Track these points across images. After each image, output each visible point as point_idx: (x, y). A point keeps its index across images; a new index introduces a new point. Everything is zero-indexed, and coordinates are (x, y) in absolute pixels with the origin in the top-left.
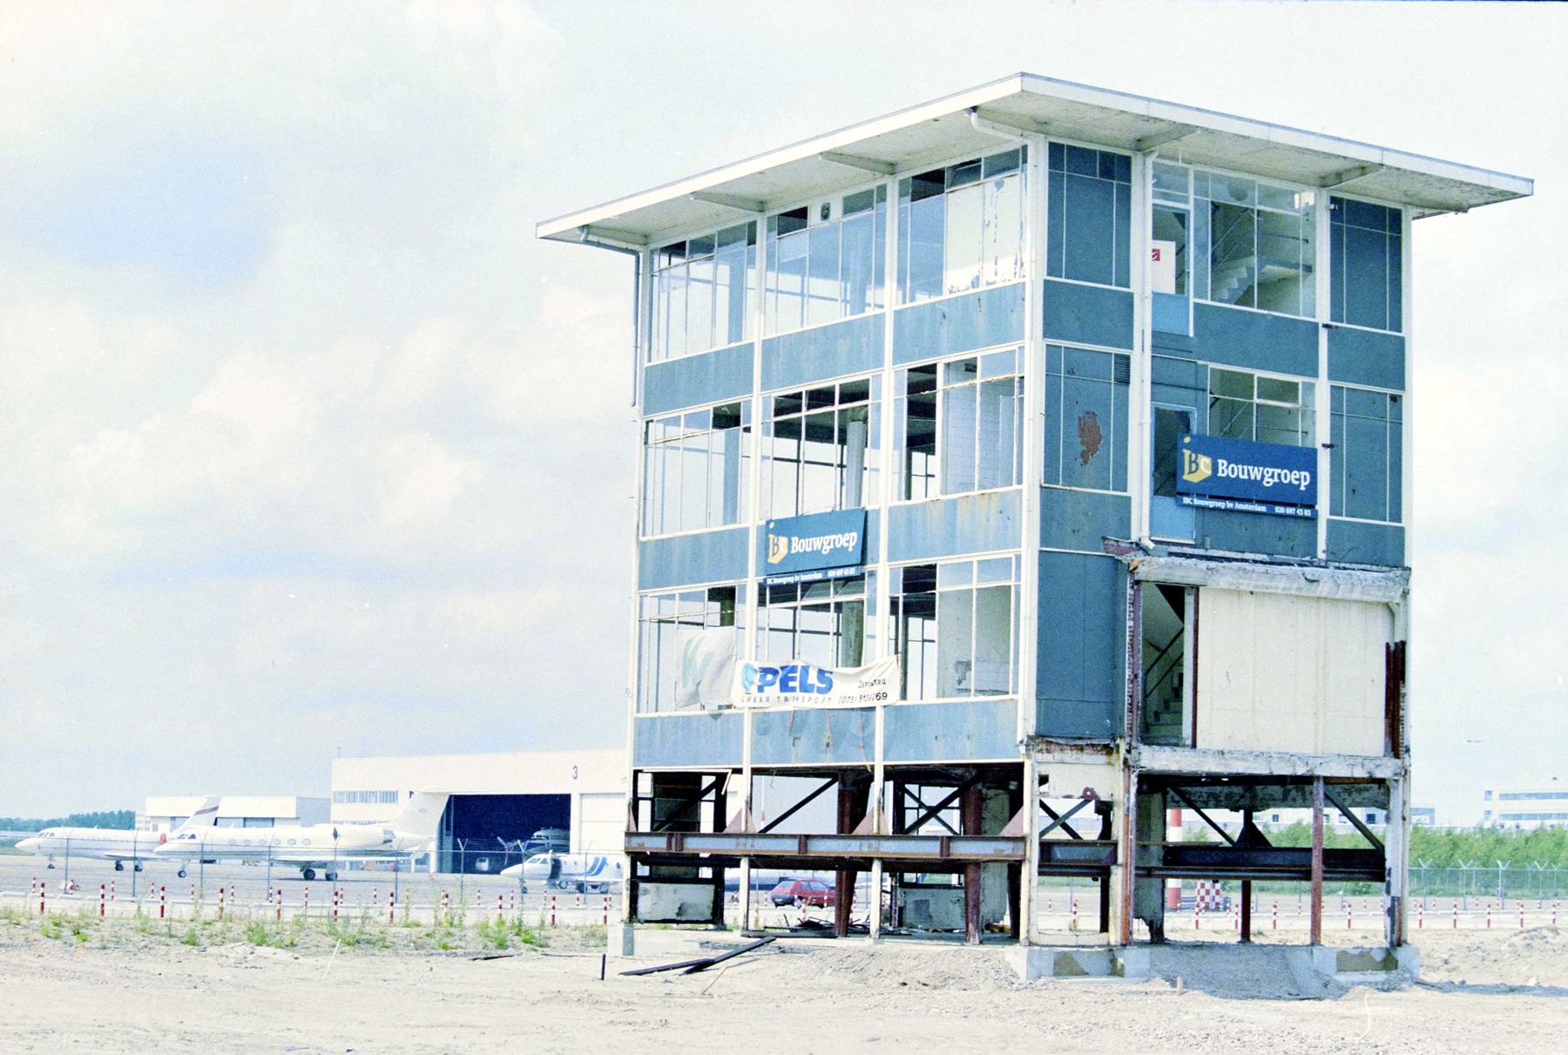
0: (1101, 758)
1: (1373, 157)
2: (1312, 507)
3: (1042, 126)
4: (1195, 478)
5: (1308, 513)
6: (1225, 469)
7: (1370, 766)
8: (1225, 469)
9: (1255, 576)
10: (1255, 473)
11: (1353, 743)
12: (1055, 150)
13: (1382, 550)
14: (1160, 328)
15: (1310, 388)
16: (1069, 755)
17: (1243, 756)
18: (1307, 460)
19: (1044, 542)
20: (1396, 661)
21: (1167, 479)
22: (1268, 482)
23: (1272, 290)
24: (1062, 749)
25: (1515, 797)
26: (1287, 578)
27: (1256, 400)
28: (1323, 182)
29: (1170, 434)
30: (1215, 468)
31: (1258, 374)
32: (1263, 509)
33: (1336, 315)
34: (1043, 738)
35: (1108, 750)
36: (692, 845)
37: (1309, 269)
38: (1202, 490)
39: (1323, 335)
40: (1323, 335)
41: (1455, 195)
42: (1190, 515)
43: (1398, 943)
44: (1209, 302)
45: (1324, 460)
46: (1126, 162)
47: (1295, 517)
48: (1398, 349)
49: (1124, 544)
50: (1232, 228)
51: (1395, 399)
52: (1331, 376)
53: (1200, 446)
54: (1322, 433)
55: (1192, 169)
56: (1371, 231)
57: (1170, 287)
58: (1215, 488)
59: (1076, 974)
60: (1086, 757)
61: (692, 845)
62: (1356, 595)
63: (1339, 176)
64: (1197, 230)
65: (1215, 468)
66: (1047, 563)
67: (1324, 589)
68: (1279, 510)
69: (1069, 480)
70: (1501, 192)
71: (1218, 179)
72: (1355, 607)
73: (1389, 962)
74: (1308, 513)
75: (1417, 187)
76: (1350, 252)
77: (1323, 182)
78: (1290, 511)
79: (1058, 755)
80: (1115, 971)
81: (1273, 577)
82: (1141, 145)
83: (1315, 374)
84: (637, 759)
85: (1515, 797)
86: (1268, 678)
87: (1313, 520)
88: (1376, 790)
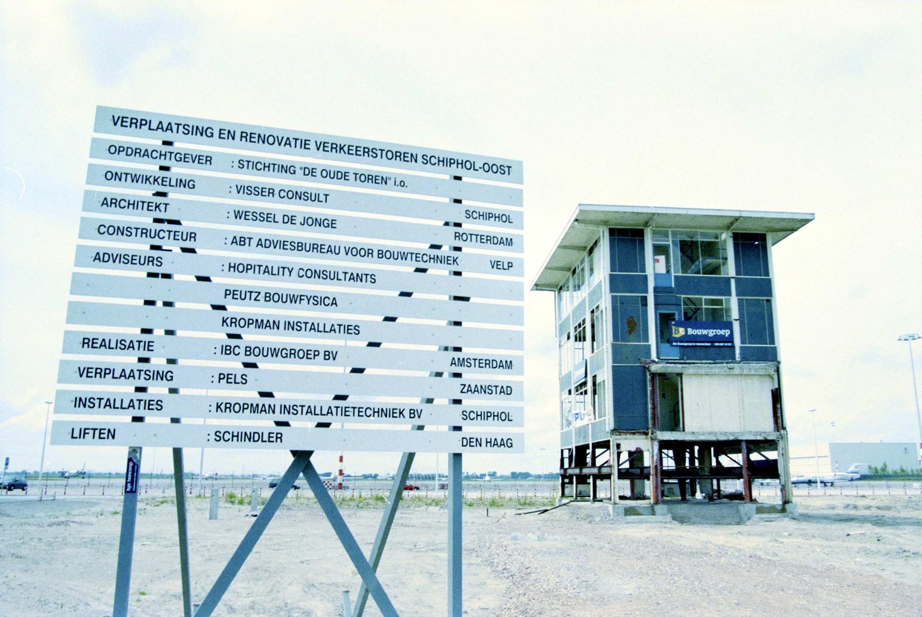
0: (644, 437)
1: (737, 214)
2: (732, 342)
3: (605, 223)
4: (677, 336)
5: (730, 344)
6: (690, 331)
7: (765, 435)
8: (690, 331)
9: (704, 367)
10: (705, 332)
11: (764, 427)
12: (612, 232)
13: (769, 355)
14: (660, 285)
15: (728, 301)
16: (628, 436)
17: (703, 434)
18: (729, 326)
19: (614, 361)
20: (777, 396)
21: (664, 335)
22: (711, 335)
23: (715, 270)
24: (626, 434)
25: (493, 443)
26: (717, 368)
27: (704, 306)
28: (728, 228)
29: (665, 321)
30: (686, 332)
31: (704, 297)
32: (716, 344)
33: (738, 273)
34: (616, 430)
35: (647, 434)
36: (586, 471)
37: (726, 259)
38: (681, 340)
39: (733, 282)
40: (733, 282)
41: (790, 225)
42: (677, 350)
43: (786, 502)
44: (680, 274)
45: (736, 326)
46: (642, 230)
47: (724, 346)
48: (768, 283)
49: (648, 361)
50: (694, 248)
51: (768, 301)
52: (737, 295)
53: (679, 324)
54: (735, 314)
55: (670, 230)
56: (753, 242)
57: (663, 271)
58: (687, 338)
59: (635, 514)
60: (636, 436)
61: (586, 471)
62: (753, 372)
63: (732, 224)
64: (675, 253)
65: (686, 332)
66: (615, 370)
67: (737, 371)
68: (716, 344)
69: (623, 340)
70: (802, 220)
71: (681, 233)
72: (756, 378)
73: (783, 510)
74: (730, 344)
75: (769, 225)
76: (743, 253)
77: (728, 228)
78: (722, 344)
79: (624, 436)
80: (653, 513)
81: (712, 368)
82: (646, 224)
83: (730, 295)
84: (562, 445)
85: (493, 443)
86: (715, 405)
87: (733, 347)
88: (771, 444)
